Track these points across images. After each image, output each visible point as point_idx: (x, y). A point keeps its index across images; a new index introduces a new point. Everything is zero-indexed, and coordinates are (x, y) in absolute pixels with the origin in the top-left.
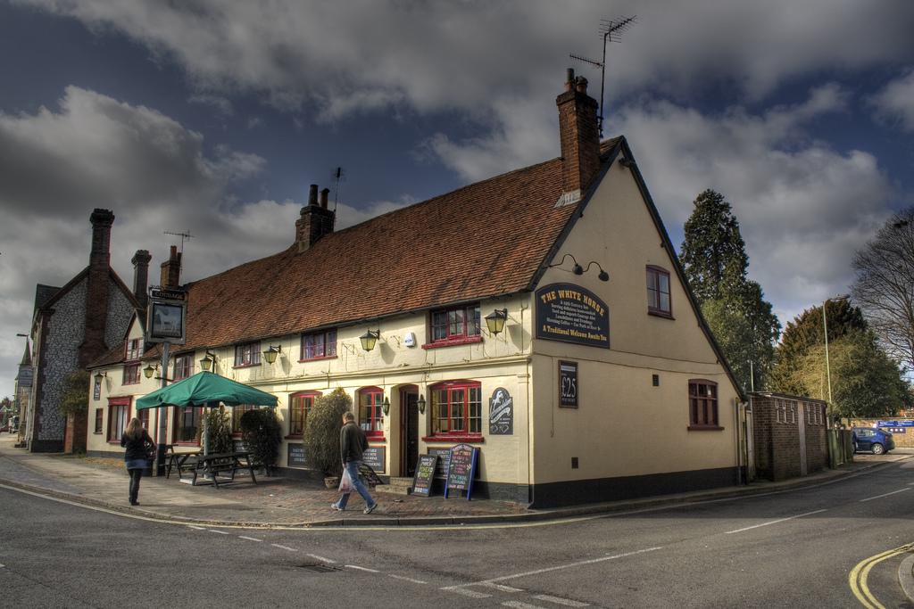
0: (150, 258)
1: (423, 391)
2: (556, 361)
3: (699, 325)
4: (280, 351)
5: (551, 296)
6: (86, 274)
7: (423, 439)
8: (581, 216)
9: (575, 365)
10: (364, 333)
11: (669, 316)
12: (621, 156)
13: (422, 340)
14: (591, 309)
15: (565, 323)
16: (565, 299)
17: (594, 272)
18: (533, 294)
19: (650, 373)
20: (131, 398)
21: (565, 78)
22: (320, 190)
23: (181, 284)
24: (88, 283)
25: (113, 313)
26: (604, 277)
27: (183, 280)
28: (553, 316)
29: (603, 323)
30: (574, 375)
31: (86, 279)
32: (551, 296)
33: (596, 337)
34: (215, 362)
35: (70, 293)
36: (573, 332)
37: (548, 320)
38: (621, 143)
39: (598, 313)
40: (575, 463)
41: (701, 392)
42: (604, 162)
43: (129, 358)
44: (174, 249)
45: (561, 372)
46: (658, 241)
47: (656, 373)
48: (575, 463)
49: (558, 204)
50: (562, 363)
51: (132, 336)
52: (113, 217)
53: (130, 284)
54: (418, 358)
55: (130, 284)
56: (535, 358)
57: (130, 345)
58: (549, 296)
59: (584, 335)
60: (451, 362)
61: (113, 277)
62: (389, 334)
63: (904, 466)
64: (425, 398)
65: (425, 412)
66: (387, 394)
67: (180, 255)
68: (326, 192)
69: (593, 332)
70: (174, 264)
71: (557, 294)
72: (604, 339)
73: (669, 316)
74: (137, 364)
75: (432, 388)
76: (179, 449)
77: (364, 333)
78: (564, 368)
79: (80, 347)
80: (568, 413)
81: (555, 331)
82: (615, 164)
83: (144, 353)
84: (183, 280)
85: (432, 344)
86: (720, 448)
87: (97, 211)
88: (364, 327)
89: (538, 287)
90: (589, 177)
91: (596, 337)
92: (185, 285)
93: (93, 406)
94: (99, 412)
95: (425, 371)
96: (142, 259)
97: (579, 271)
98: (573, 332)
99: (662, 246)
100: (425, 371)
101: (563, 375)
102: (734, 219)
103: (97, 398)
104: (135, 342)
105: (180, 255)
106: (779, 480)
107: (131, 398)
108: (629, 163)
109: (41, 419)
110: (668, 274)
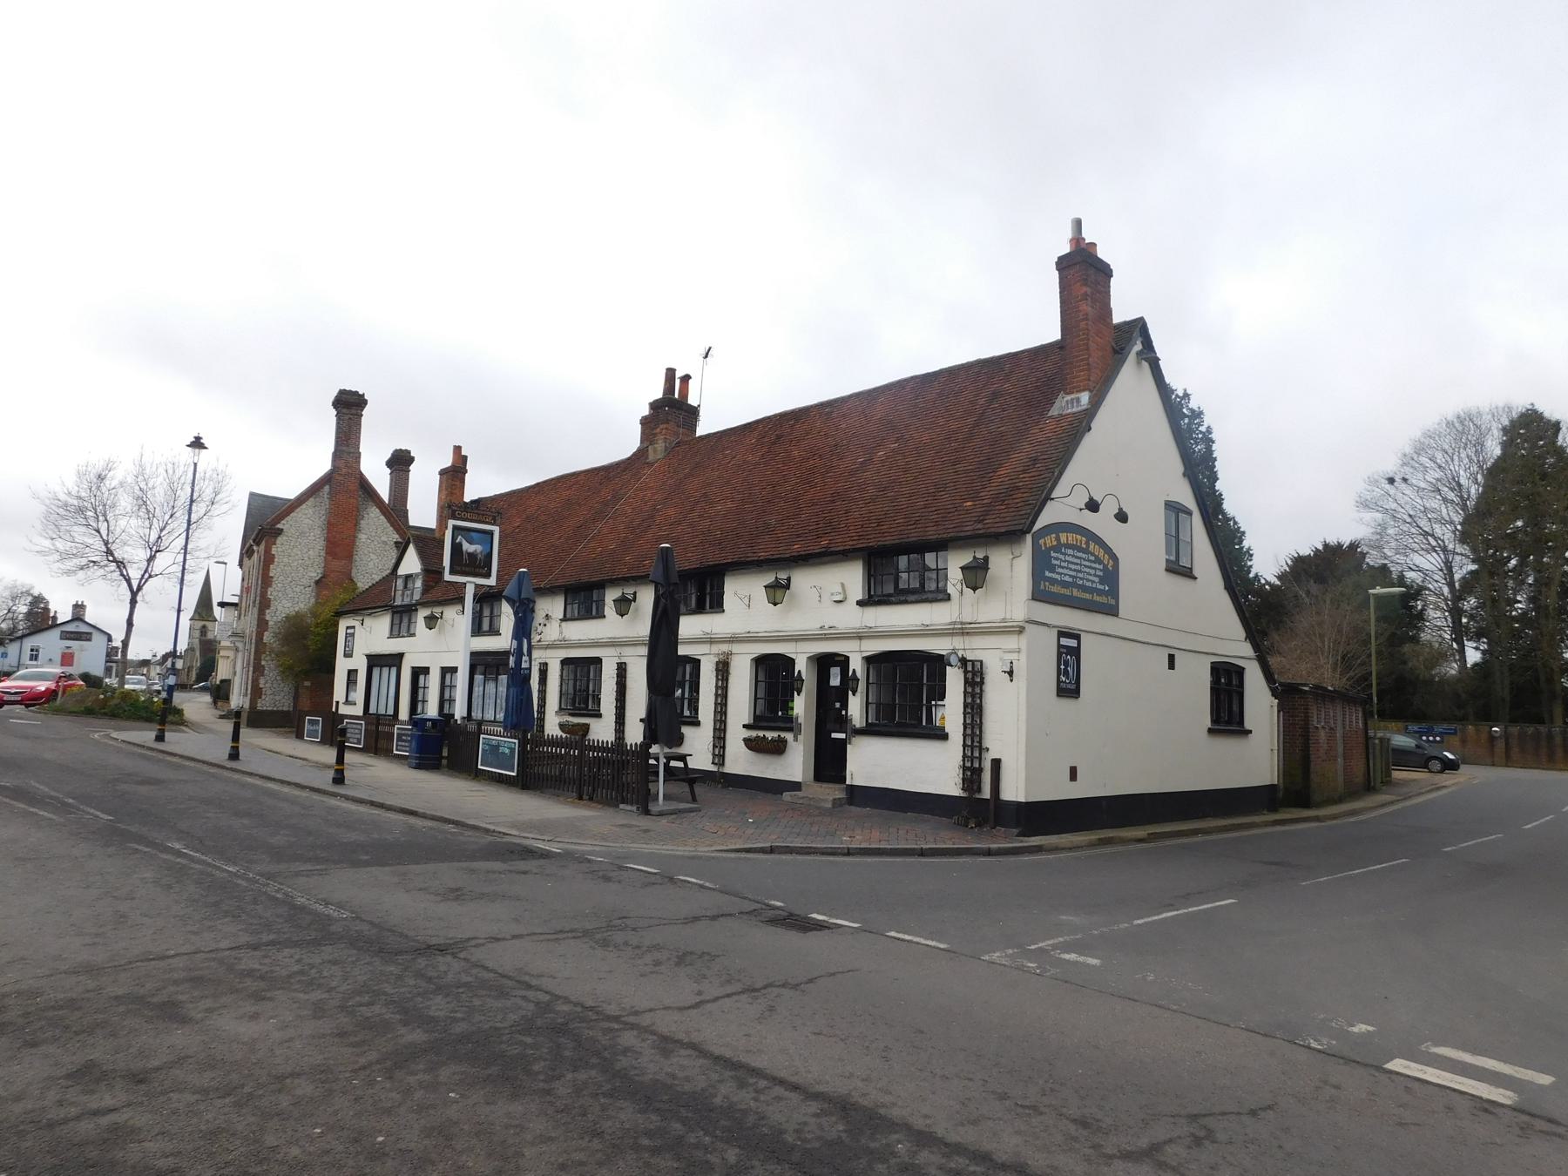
0: (412, 459)
2: (1054, 633)
5: (1050, 541)
6: (326, 480)
9: (1077, 637)
10: (769, 578)
11: (1188, 574)
13: (857, 590)
14: (1098, 560)
15: (1067, 579)
16: (1068, 546)
17: (1108, 509)
18: (1029, 538)
19: (1165, 653)
20: (401, 656)
21: (1068, 234)
22: (679, 374)
23: (467, 498)
26: (1122, 517)
28: (1052, 570)
29: (1111, 577)
30: (1076, 652)
31: (327, 488)
32: (1050, 541)
33: (1103, 599)
36: (1075, 592)
37: (1047, 574)
38: (1138, 328)
39: (1105, 566)
41: (1226, 682)
42: (1118, 354)
44: (457, 449)
45: (1060, 646)
49: (1054, 411)
50: (1062, 634)
51: (403, 570)
52: (365, 402)
54: (852, 617)
56: (1030, 628)
57: (400, 583)
58: (1048, 539)
59: (1087, 596)
60: (906, 625)
62: (805, 581)
63: (1015, 831)
64: (859, 674)
69: (1100, 593)
70: (454, 475)
71: (1058, 539)
72: (1113, 602)
73: (1188, 574)
75: (870, 660)
77: (769, 578)
78: (1064, 641)
79: (317, 582)
80: (1067, 703)
81: (1054, 589)
82: (1132, 357)
85: (871, 600)
86: (1255, 759)
87: (342, 392)
88: (769, 570)
89: (1036, 528)
91: (1103, 599)
92: (473, 502)
93: (342, 666)
94: (352, 674)
95: (859, 637)
96: (400, 462)
97: (1093, 506)
98: (1075, 592)
100: (859, 637)
101: (1062, 651)
102: (1209, 430)
103: (348, 655)
104: (408, 577)
106: (1319, 805)
107: (401, 656)
109: (262, 681)
110: (1190, 513)
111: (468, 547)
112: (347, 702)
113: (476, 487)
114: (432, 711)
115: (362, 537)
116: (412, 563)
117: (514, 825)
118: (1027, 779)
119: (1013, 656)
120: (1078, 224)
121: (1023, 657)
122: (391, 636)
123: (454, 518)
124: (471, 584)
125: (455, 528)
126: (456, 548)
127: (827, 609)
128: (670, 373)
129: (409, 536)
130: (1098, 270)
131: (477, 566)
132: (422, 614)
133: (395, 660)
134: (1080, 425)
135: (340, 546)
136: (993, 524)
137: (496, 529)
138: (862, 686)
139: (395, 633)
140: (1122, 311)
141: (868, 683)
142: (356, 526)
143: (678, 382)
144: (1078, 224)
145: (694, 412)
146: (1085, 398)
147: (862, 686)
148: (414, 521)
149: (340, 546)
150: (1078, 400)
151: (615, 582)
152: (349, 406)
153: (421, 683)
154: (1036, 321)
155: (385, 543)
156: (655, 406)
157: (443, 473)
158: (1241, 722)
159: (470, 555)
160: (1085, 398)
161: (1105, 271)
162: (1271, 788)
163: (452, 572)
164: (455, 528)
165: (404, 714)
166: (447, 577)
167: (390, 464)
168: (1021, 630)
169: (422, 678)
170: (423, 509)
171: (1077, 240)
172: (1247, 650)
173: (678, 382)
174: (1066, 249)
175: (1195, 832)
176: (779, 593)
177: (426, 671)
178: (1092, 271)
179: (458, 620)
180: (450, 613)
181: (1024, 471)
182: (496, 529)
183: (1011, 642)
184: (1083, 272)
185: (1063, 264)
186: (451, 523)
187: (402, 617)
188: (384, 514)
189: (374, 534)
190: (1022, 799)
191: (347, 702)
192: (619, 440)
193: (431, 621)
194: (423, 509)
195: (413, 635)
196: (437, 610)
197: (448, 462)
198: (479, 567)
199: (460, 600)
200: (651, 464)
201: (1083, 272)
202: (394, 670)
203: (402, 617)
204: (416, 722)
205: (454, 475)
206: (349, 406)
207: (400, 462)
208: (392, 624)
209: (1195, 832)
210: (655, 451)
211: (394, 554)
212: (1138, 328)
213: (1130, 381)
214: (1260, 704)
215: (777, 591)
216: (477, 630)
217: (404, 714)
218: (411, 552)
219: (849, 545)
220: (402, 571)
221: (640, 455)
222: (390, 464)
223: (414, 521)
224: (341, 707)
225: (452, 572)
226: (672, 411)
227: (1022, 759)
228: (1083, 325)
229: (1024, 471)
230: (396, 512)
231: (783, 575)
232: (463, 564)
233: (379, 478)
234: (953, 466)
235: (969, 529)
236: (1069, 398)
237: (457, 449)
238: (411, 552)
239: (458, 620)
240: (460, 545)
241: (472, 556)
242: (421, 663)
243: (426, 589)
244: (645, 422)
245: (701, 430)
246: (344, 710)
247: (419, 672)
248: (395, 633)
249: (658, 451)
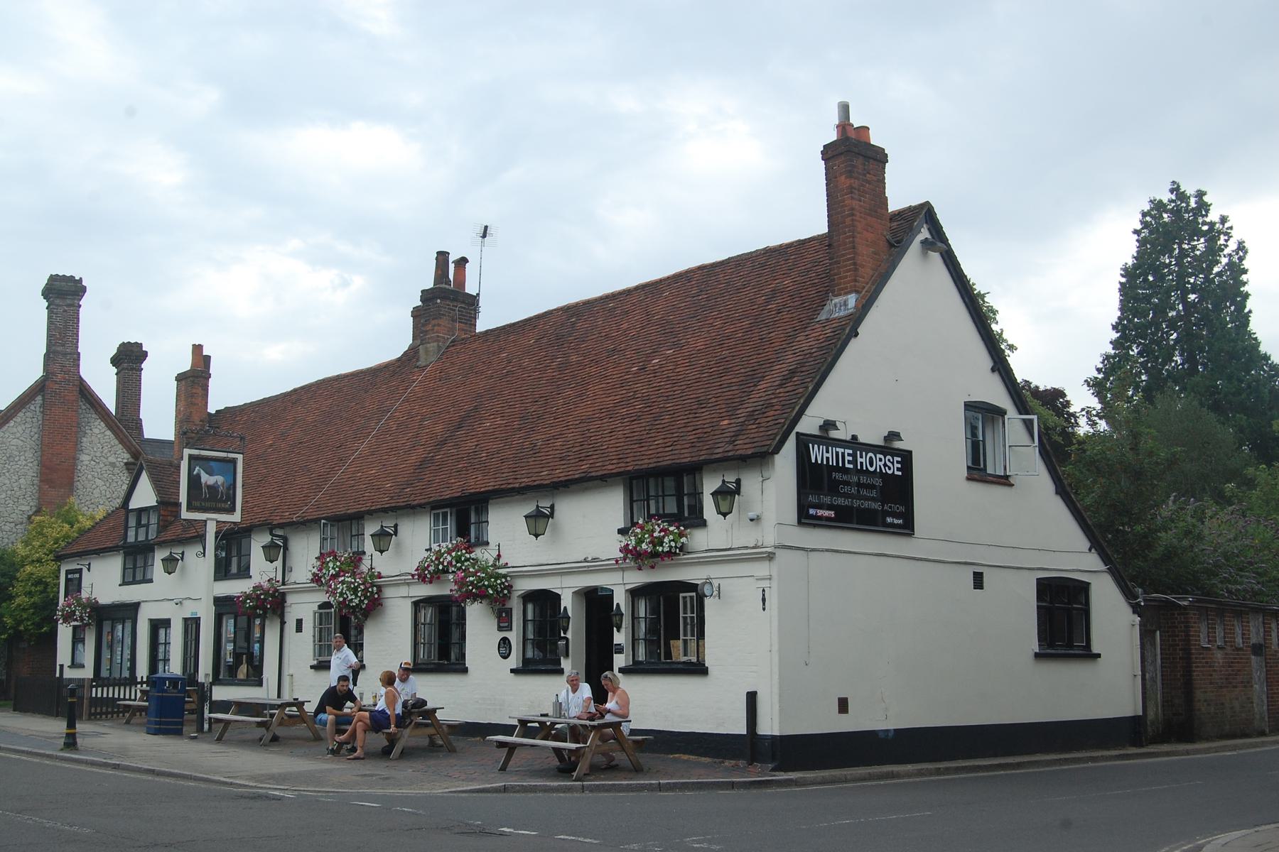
1: (620, 599)
3: (1057, 493)
4: (396, 533)
7: (621, 670)
8: (857, 334)
10: (529, 508)
12: (924, 234)
20: (135, 607)
22: (452, 258)
24: (43, 406)
25: (88, 458)
27: (218, 400)
31: (39, 398)
34: (286, 548)
35: (12, 423)
38: (926, 213)
40: (843, 705)
43: (131, 539)
44: (197, 349)
46: (987, 363)
47: (979, 570)
48: (843, 705)
49: (823, 316)
52: (84, 290)
53: (110, 402)
55: (110, 402)
56: (779, 552)
61: (86, 394)
64: (623, 609)
65: (623, 630)
66: (567, 602)
67: (208, 358)
68: (462, 262)
70: (195, 380)
74: (146, 549)
75: (635, 594)
76: (220, 693)
82: (915, 246)
83: (159, 532)
84: (218, 400)
87: (53, 279)
90: (871, 273)
99: (993, 370)
104: (141, 511)
105: (208, 358)
107: (135, 607)
108: (938, 241)
110: (1002, 413)
111: (206, 479)
112: (75, 665)
113: (223, 394)
114: (175, 667)
115: (85, 458)
116: (145, 496)
117: (252, 778)
118: (781, 710)
119: (765, 584)
120: (845, 109)
121: (775, 584)
122: (124, 583)
123: (188, 445)
124: (213, 522)
125: (191, 457)
126: (194, 482)
127: (587, 539)
128: (442, 257)
129: (144, 457)
130: (867, 157)
131: (219, 500)
132: (160, 555)
133: (129, 611)
134: (850, 328)
135: (57, 474)
136: (743, 447)
137: (240, 457)
138: (626, 622)
139: (129, 579)
140: (900, 193)
141: (634, 618)
142: (77, 447)
143: (452, 267)
144: (845, 109)
145: (472, 302)
146: (852, 300)
147: (626, 622)
148: (149, 433)
149: (57, 474)
150: (845, 304)
151: (372, 513)
152: (64, 295)
153: (162, 639)
154: (803, 214)
155: (113, 465)
156: (427, 296)
157: (181, 378)
158: (1088, 646)
159: (209, 487)
160: (852, 300)
161: (878, 158)
162: (1134, 721)
163: (190, 508)
164: (191, 457)
165: (142, 671)
166: (185, 514)
167: (115, 361)
168: (770, 557)
169: (162, 632)
170: (159, 418)
171: (844, 126)
172: (1093, 561)
173: (452, 267)
174: (832, 136)
175: (1019, 766)
176: (541, 522)
177: (166, 623)
178: (859, 162)
179: (199, 565)
180: (191, 553)
181: (780, 386)
182: (240, 457)
183: (762, 569)
184: (853, 160)
185: (830, 153)
186: (187, 452)
187: (137, 562)
188: (110, 427)
189: (100, 456)
190: (777, 733)
191: (75, 665)
192: (384, 335)
193: (171, 564)
194: (159, 418)
195: (151, 581)
196: (177, 551)
197: (186, 365)
198: (221, 501)
199: (201, 538)
200: (423, 368)
201: (853, 160)
202: (128, 625)
203: (137, 562)
204: (154, 681)
205: (195, 380)
206: (64, 295)
207: (129, 359)
208: (125, 569)
209: (1019, 766)
210: (427, 351)
211: (125, 479)
212: (926, 213)
213: (915, 275)
214: (1113, 618)
215: (538, 522)
216: (222, 571)
217: (142, 671)
218: (144, 480)
219: (611, 468)
220: (134, 504)
221: (410, 356)
222: (115, 361)
223: (149, 433)
224: (66, 669)
225: (190, 508)
226: (446, 301)
227: (776, 690)
228: (848, 221)
229: (780, 386)
230: (126, 421)
231: (545, 504)
232: (203, 498)
233: (102, 380)
234: (711, 381)
235: (719, 452)
236: (836, 300)
237: (197, 349)
238: (144, 480)
239: (199, 565)
240: (199, 476)
241: (213, 489)
242: (160, 612)
243: (163, 527)
244: (416, 313)
245: (482, 325)
246: (69, 674)
247: (158, 626)
248: (129, 579)
249: (428, 357)
